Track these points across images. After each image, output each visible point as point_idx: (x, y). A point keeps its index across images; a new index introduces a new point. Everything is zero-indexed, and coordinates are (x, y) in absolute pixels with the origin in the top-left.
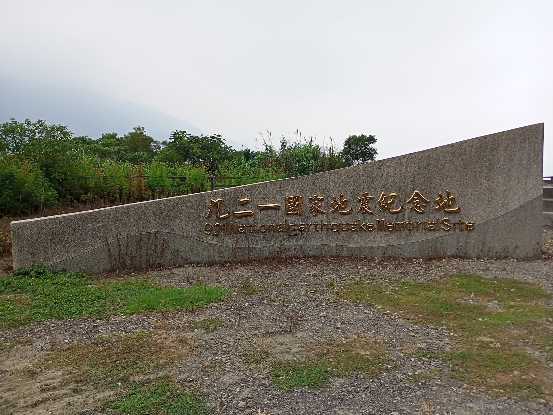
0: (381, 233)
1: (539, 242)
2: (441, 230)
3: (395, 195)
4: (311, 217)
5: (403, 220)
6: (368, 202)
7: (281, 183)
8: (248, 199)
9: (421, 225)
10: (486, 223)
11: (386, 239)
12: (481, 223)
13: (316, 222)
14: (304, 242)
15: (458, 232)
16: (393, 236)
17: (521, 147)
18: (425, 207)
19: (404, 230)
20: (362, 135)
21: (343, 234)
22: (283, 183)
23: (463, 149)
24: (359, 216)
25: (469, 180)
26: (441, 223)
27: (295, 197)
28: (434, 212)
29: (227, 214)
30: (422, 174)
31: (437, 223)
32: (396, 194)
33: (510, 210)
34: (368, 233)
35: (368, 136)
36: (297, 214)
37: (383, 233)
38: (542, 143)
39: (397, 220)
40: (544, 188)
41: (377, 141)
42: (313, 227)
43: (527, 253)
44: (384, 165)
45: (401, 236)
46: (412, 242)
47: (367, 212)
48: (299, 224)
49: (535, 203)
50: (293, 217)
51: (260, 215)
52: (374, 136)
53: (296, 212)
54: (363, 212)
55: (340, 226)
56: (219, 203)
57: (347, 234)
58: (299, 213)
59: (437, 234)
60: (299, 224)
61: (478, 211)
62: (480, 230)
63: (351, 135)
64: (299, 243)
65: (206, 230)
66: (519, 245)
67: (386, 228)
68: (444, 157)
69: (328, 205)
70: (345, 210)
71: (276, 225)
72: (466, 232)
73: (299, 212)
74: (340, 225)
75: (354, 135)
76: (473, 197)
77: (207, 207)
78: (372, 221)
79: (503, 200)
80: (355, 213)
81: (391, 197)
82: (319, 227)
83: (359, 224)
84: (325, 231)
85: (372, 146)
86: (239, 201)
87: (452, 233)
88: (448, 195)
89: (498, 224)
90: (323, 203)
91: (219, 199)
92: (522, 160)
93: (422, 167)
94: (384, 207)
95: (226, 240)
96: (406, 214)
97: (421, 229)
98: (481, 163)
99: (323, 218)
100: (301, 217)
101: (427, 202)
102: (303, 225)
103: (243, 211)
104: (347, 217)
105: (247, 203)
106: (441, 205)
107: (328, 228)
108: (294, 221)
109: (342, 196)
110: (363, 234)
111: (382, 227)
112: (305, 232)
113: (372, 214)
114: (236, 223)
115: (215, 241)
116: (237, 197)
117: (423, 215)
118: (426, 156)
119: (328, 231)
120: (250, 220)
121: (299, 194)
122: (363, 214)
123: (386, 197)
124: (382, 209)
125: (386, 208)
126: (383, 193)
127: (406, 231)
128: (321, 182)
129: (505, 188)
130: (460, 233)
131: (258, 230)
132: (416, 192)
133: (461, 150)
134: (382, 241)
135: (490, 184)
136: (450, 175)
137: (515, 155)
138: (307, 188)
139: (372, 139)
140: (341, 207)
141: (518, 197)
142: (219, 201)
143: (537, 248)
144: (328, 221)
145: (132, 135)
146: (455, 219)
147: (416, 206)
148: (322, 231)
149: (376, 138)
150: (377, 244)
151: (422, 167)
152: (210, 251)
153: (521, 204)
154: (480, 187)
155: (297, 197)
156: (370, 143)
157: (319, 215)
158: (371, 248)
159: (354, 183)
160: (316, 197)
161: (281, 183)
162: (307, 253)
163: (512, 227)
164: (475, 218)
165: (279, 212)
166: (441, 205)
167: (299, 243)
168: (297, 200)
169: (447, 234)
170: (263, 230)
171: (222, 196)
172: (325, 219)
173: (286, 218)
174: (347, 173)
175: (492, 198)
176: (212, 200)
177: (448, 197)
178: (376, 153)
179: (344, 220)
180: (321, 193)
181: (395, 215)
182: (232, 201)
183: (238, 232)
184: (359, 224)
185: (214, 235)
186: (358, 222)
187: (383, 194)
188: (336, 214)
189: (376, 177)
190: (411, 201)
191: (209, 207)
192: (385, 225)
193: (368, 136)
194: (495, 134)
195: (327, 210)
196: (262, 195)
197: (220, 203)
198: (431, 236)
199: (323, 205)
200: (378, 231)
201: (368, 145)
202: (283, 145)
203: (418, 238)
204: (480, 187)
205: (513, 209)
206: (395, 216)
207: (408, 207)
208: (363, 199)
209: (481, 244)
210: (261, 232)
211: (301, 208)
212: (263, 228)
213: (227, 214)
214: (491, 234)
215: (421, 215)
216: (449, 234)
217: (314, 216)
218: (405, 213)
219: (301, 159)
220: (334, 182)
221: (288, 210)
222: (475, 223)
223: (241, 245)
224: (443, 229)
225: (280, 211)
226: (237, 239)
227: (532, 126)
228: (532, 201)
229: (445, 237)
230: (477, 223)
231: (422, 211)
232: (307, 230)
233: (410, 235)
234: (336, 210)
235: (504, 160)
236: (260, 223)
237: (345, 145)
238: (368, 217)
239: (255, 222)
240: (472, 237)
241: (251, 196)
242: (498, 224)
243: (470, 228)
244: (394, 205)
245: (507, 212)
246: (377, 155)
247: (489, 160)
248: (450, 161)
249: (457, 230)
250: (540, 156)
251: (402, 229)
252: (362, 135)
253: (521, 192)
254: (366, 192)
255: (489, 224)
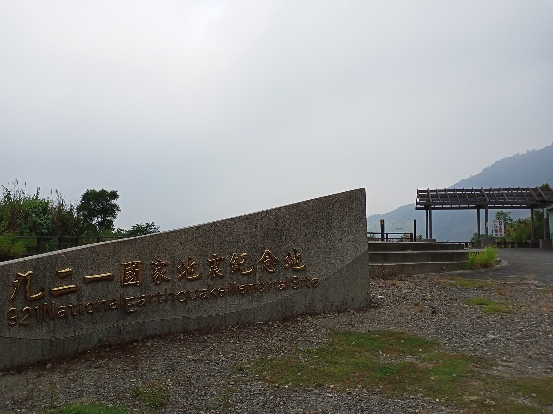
0: (233, 297)
1: (368, 292)
2: (290, 288)
3: (247, 255)
4: (153, 287)
5: (255, 281)
6: (219, 264)
7: (115, 247)
8: (71, 270)
9: (272, 286)
10: (328, 279)
11: (237, 303)
12: (323, 278)
13: (159, 293)
14: (144, 319)
15: (305, 289)
16: (245, 300)
17: (350, 208)
18: (275, 266)
19: (255, 292)
20: (102, 189)
21: (191, 304)
22: (117, 246)
23: (305, 209)
24: (209, 281)
25: (312, 238)
26: (290, 282)
27: (133, 264)
28: (283, 271)
29: (41, 293)
30: (271, 232)
31: (286, 282)
32: (247, 254)
33: (345, 265)
34: (219, 299)
35: (109, 192)
36: (136, 284)
37: (235, 298)
38: (365, 205)
39: (249, 282)
40: (368, 243)
41: (120, 197)
42: (155, 299)
43: (360, 304)
44: (234, 223)
45: (253, 299)
46: (264, 304)
47: (218, 275)
48: (137, 297)
49: (363, 257)
50: (130, 289)
51: (87, 291)
52: (117, 191)
53: (135, 282)
54: (214, 276)
55: (187, 295)
56: (29, 278)
57: (196, 303)
58: (138, 283)
59: (287, 294)
60: (137, 297)
61: (320, 268)
62: (323, 285)
63: (89, 189)
64: (138, 321)
65: (9, 319)
66: (353, 297)
67: (238, 291)
68: (289, 216)
69: (173, 270)
70: (193, 275)
71: (108, 301)
72: (312, 288)
73: (138, 282)
74: (188, 292)
75: (92, 189)
76: (315, 254)
77: (11, 284)
78: (223, 285)
79: (339, 256)
80: (205, 278)
81: (242, 258)
82: (162, 298)
83: (209, 290)
84: (170, 302)
85: (114, 202)
86: (57, 273)
87: (299, 291)
88: (296, 252)
89: (337, 278)
90: (168, 268)
91: (30, 272)
92: (352, 219)
93: (270, 226)
94: (236, 269)
95: (38, 331)
96: (257, 275)
97: (271, 289)
98: (321, 222)
99: (168, 286)
100: (140, 288)
101: (277, 262)
102: (143, 297)
103: (63, 286)
104: (196, 284)
105: (69, 274)
106: (289, 263)
107: (174, 299)
108: (131, 295)
109: (190, 259)
110: (213, 301)
111: (234, 291)
112: (145, 306)
113: (222, 277)
114: (53, 303)
115: (22, 334)
116: (55, 268)
117: (274, 275)
118: (274, 215)
119: (173, 302)
120: (73, 299)
121: (138, 259)
122: (213, 277)
123: (237, 257)
124: (233, 270)
125: (238, 270)
126: (234, 253)
127: (258, 293)
128: (165, 244)
129: (340, 245)
130: (306, 290)
131: (84, 311)
132: (266, 251)
133: (304, 209)
134: (234, 306)
135: (329, 242)
136: (296, 233)
137: (346, 216)
138: (148, 251)
139: (114, 195)
140: (189, 272)
141: (351, 253)
142: (29, 274)
143: (368, 298)
144: (173, 290)
145: (542, 186)
146: (301, 277)
147: (267, 266)
148: (166, 302)
149: (118, 193)
150: (228, 311)
151: (270, 226)
152: (14, 349)
153: (353, 259)
154: (321, 244)
155: (136, 262)
156: (112, 199)
157: (163, 284)
158: (221, 316)
159: (203, 243)
160: (159, 262)
161: (115, 247)
162: (149, 333)
163: (348, 281)
164: (318, 275)
165: (112, 285)
166: (289, 263)
167: (138, 321)
168: (136, 267)
169: (296, 292)
170: (90, 310)
171: (33, 268)
172: (170, 287)
173: (121, 291)
174: (195, 232)
175: (331, 255)
176: (19, 274)
177: (296, 255)
178: (118, 209)
179: (191, 287)
180: (165, 257)
181: (246, 276)
182: (48, 274)
183: (56, 317)
184: (209, 290)
185: (21, 325)
186: (207, 287)
187: (235, 255)
188: (183, 281)
189: (226, 237)
190: (262, 261)
191: (14, 285)
192: (236, 288)
193: (109, 192)
194: (330, 196)
195: (172, 277)
196: (90, 263)
197: (31, 278)
198: (282, 295)
199: (167, 271)
200: (229, 295)
201: (109, 200)
202: (7, 197)
203: (269, 299)
204: (321, 244)
205: (347, 263)
206: (246, 278)
207: (259, 267)
208: (214, 261)
209: (444, 296)
210: (88, 313)
211: (140, 276)
212: (90, 308)
213: (41, 293)
214: (332, 289)
215: (272, 275)
216: (297, 292)
217: (156, 285)
218: (256, 274)
219: (27, 216)
220: (181, 243)
221: (124, 279)
222: (319, 280)
223: (61, 335)
224: (292, 287)
225: (114, 283)
226: (54, 327)
227: (357, 190)
228: (360, 256)
229: (294, 295)
230: (320, 279)
231: (272, 271)
232: (148, 304)
233: (262, 296)
234: (184, 276)
235: (338, 219)
236: (87, 301)
237: (82, 200)
238: (219, 281)
239: (79, 300)
240: (317, 293)
241: (74, 265)
242: (337, 278)
243: (315, 285)
244: (246, 266)
245: (343, 266)
246: (119, 212)
247: (327, 220)
248: (295, 220)
249: (305, 287)
250: (364, 216)
251: (254, 291)
252: (102, 189)
253: (352, 248)
254: (217, 253)
255: (330, 279)
